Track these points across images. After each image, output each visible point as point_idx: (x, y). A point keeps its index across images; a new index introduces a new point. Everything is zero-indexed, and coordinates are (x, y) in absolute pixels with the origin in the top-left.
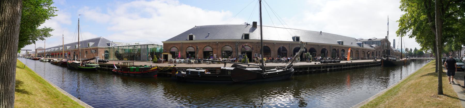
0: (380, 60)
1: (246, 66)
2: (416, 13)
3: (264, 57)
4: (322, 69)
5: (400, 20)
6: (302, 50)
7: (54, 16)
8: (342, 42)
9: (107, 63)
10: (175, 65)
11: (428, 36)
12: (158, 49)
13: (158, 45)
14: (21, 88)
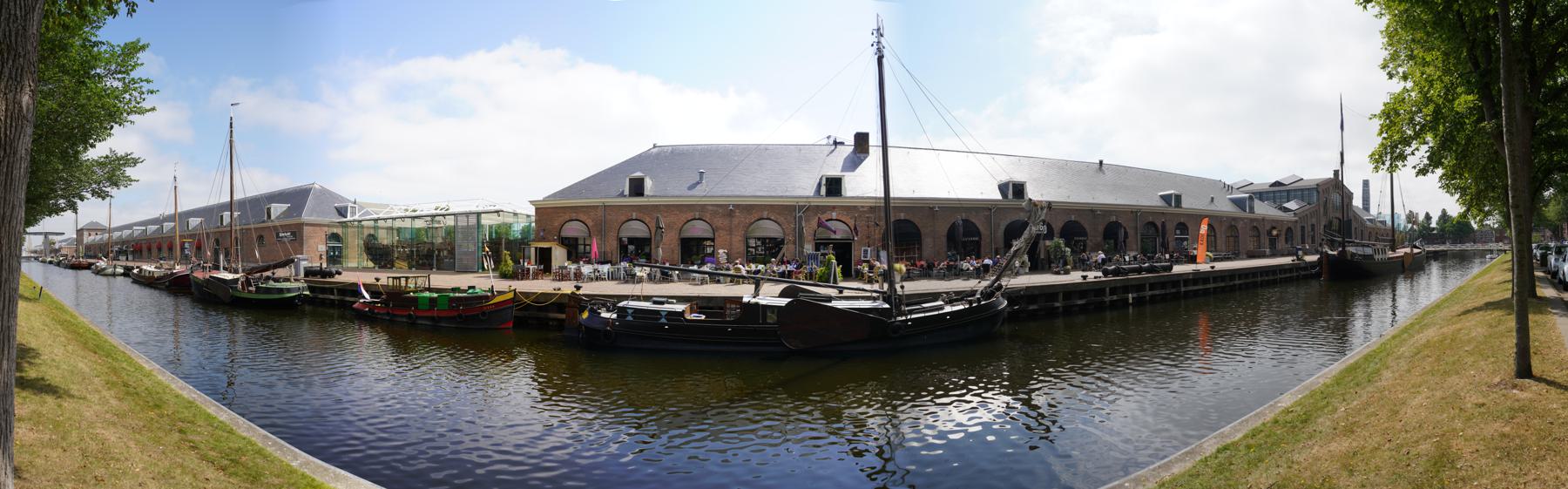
0: (1315, 258)
1: (833, 292)
2: (1438, 85)
3: (897, 261)
4: (1108, 299)
5: (1383, 112)
6: (1034, 229)
7: (142, 112)
8: (1178, 198)
9: (338, 278)
10: (578, 288)
11: (1484, 169)
12: (517, 228)
14: (32, 373)
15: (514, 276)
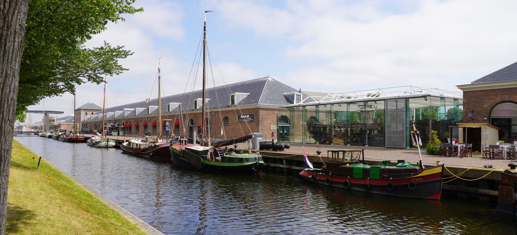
7: (131, 11)
9: (286, 151)
12: (443, 112)
13: (442, 98)
15: (441, 153)
